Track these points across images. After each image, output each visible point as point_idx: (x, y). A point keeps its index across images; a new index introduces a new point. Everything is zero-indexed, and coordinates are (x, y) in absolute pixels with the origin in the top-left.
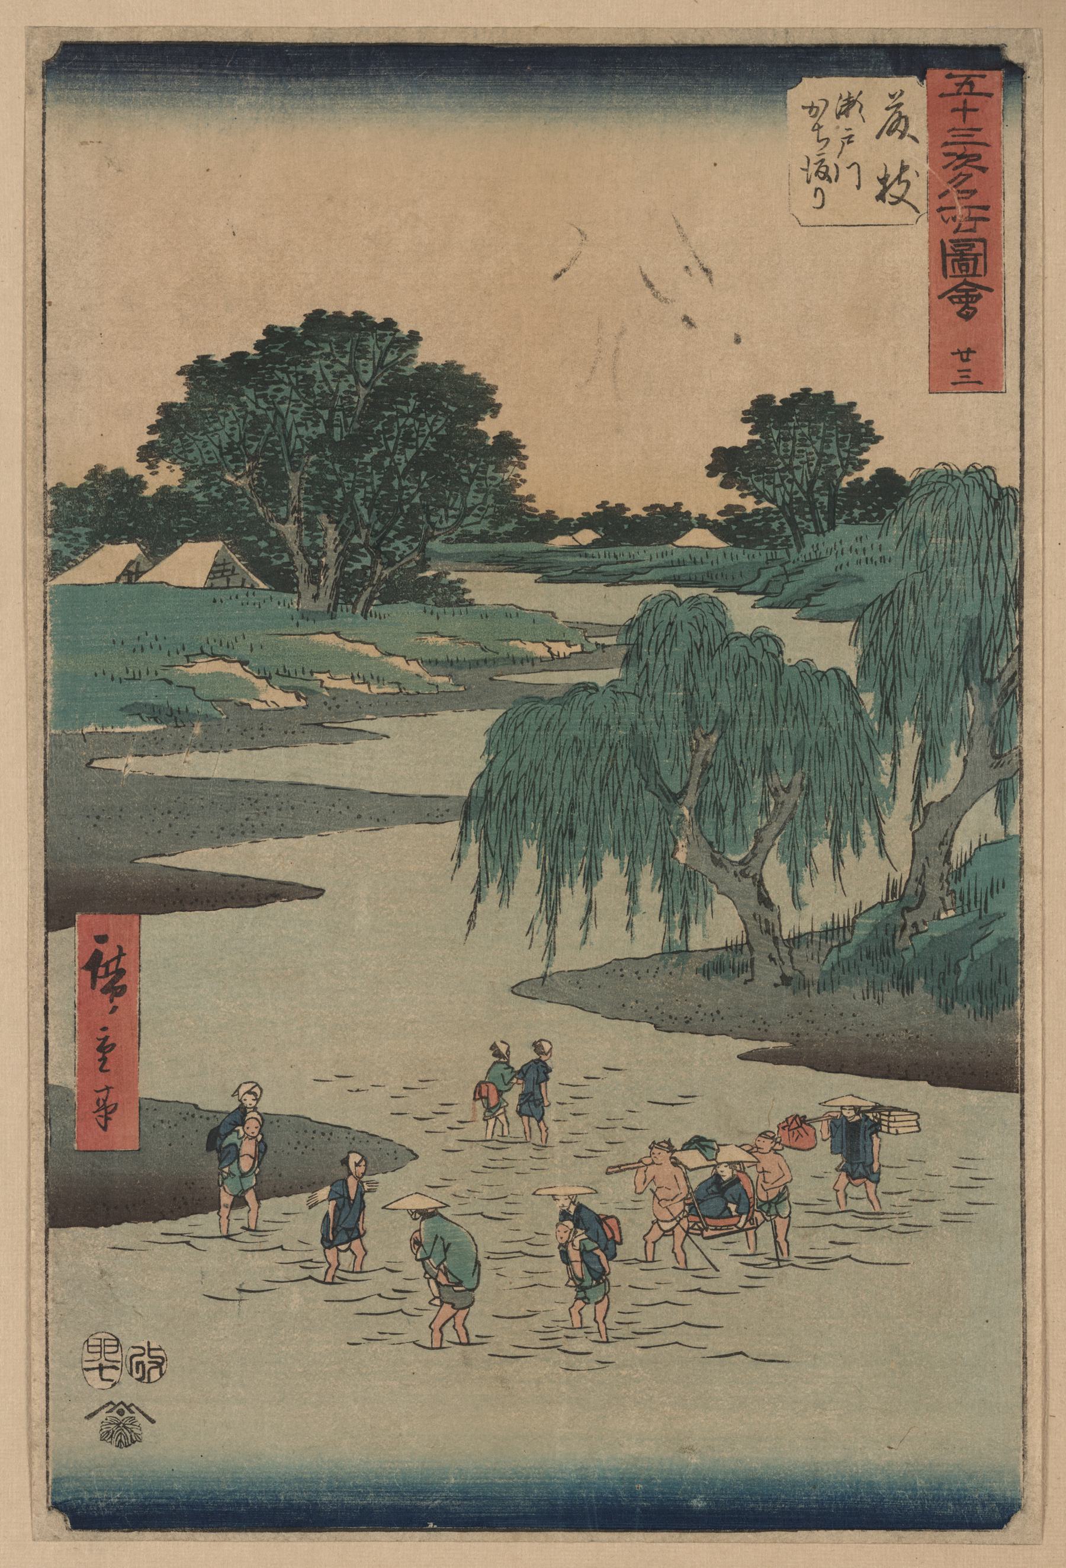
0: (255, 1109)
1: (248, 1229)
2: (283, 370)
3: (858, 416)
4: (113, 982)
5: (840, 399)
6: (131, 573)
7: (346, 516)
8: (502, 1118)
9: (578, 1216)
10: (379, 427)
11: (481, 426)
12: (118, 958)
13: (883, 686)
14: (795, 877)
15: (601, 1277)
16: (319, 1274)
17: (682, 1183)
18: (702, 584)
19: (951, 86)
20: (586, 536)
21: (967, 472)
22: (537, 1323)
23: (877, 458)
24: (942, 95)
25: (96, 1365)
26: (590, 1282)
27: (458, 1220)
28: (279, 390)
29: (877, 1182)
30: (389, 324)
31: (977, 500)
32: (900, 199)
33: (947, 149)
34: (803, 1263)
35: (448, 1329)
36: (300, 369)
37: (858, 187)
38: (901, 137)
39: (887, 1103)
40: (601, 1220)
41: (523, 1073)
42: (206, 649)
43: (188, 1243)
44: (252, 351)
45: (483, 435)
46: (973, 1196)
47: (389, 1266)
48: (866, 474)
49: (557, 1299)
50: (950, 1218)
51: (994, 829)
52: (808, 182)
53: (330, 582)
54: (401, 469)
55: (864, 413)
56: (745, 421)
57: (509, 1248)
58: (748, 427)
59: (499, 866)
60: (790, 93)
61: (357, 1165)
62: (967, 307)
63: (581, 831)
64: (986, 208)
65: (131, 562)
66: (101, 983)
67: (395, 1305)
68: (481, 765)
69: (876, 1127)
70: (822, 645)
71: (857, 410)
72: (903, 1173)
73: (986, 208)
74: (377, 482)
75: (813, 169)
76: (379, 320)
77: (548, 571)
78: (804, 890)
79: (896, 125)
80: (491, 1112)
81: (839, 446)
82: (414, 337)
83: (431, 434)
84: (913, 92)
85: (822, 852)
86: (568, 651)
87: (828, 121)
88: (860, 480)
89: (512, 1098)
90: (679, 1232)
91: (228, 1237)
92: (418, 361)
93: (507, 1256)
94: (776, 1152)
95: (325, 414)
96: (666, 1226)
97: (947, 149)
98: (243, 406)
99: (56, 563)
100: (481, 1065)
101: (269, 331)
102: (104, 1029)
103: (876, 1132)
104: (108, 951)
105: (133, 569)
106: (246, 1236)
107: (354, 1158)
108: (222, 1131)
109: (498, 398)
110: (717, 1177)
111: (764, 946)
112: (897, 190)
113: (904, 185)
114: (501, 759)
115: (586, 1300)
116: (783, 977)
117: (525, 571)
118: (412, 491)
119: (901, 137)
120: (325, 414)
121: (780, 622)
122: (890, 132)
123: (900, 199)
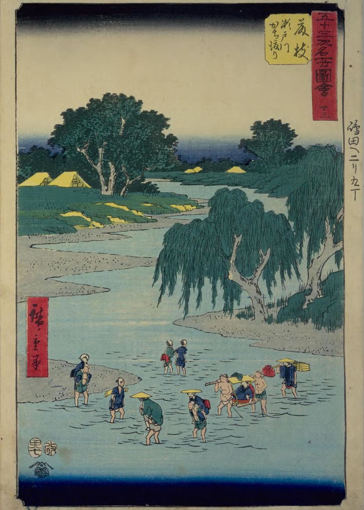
0: (87, 363)
1: (84, 404)
2: (97, 113)
3: (290, 128)
4: (39, 320)
5: (283, 122)
6: (46, 182)
7: (117, 163)
8: (170, 366)
9: (196, 399)
10: (128, 132)
11: (163, 132)
12: (41, 312)
13: (297, 220)
14: (269, 286)
15: (202, 419)
16: (109, 420)
17: (231, 388)
18: (237, 185)
19: (320, 17)
20: (198, 169)
21: (326, 147)
22: (181, 436)
23: (296, 142)
24: (317, 20)
25: (33, 449)
26: (201, 423)
27: (156, 401)
28: (95, 120)
29: (296, 388)
30: (132, 98)
31: (330, 157)
32: (303, 56)
33: (318, 38)
34: (271, 415)
35: (152, 439)
36: (102, 113)
37: (288, 52)
38: (303, 35)
39: (298, 360)
40: (204, 401)
41: (177, 351)
42: (70, 208)
43: (64, 409)
44: (86, 107)
45: (164, 135)
46: (329, 392)
47: (132, 417)
48: (292, 147)
49: (188, 427)
50: (320, 400)
51: (336, 269)
52: (271, 50)
53: (112, 185)
54: (136, 147)
55: (292, 127)
56: (252, 130)
57: (173, 411)
58: (253, 132)
59: (168, 281)
60: (266, 20)
61: (121, 382)
62: (324, 92)
63: (197, 268)
64: (331, 58)
65: (45, 179)
66: (35, 320)
67: (134, 430)
68: (162, 247)
69: (294, 369)
70: (277, 206)
71: (289, 126)
72: (306, 385)
73: (331, 58)
74: (128, 151)
75: (273, 45)
76: (128, 96)
77: (185, 182)
78: (272, 289)
79: (302, 30)
80: (166, 365)
81: (283, 138)
82: (140, 102)
83: (146, 135)
84: (307, 19)
85: (277, 275)
86: (191, 208)
87: (278, 28)
88: (290, 150)
89: (174, 359)
90: (229, 405)
91: (78, 407)
92: (142, 110)
93: (172, 414)
94: (262, 378)
95: (110, 128)
96: (225, 403)
97: (318, 38)
98: (83, 126)
99: (20, 179)
100: (163, 349)
101: (92, 100)
102: (36, 336)
103: (295, 371)
104: (38, 310)
105: (46, 180)
106: (84, 406)
107: (120, 380)
108: (76, 371)
109: (168, 123)
110: (243, 386)
111: (258, 308)
112: (301, 52)
113: (303, 51)
114: (170, 245)
115: (199, 428)
116: (265, 318)
117: (177, 181)
118: (139, 154)
119: (303, 35)
120: (110, 128)
121: (264, 198)
122: (299, 33)
123: (303, 56)
